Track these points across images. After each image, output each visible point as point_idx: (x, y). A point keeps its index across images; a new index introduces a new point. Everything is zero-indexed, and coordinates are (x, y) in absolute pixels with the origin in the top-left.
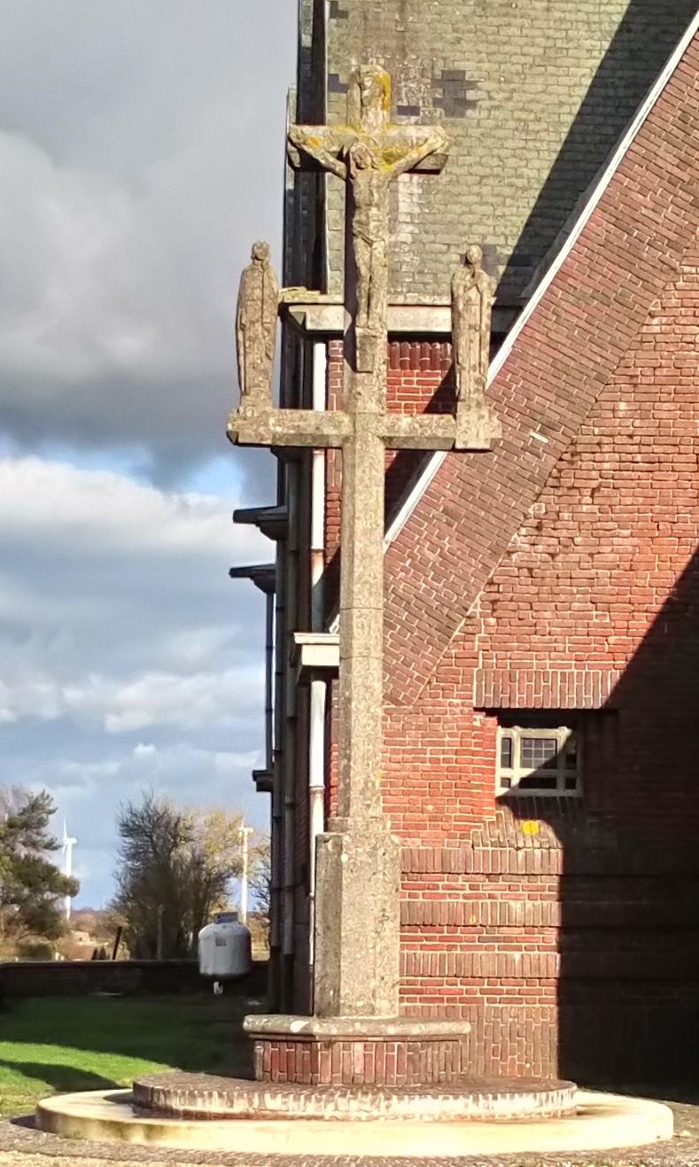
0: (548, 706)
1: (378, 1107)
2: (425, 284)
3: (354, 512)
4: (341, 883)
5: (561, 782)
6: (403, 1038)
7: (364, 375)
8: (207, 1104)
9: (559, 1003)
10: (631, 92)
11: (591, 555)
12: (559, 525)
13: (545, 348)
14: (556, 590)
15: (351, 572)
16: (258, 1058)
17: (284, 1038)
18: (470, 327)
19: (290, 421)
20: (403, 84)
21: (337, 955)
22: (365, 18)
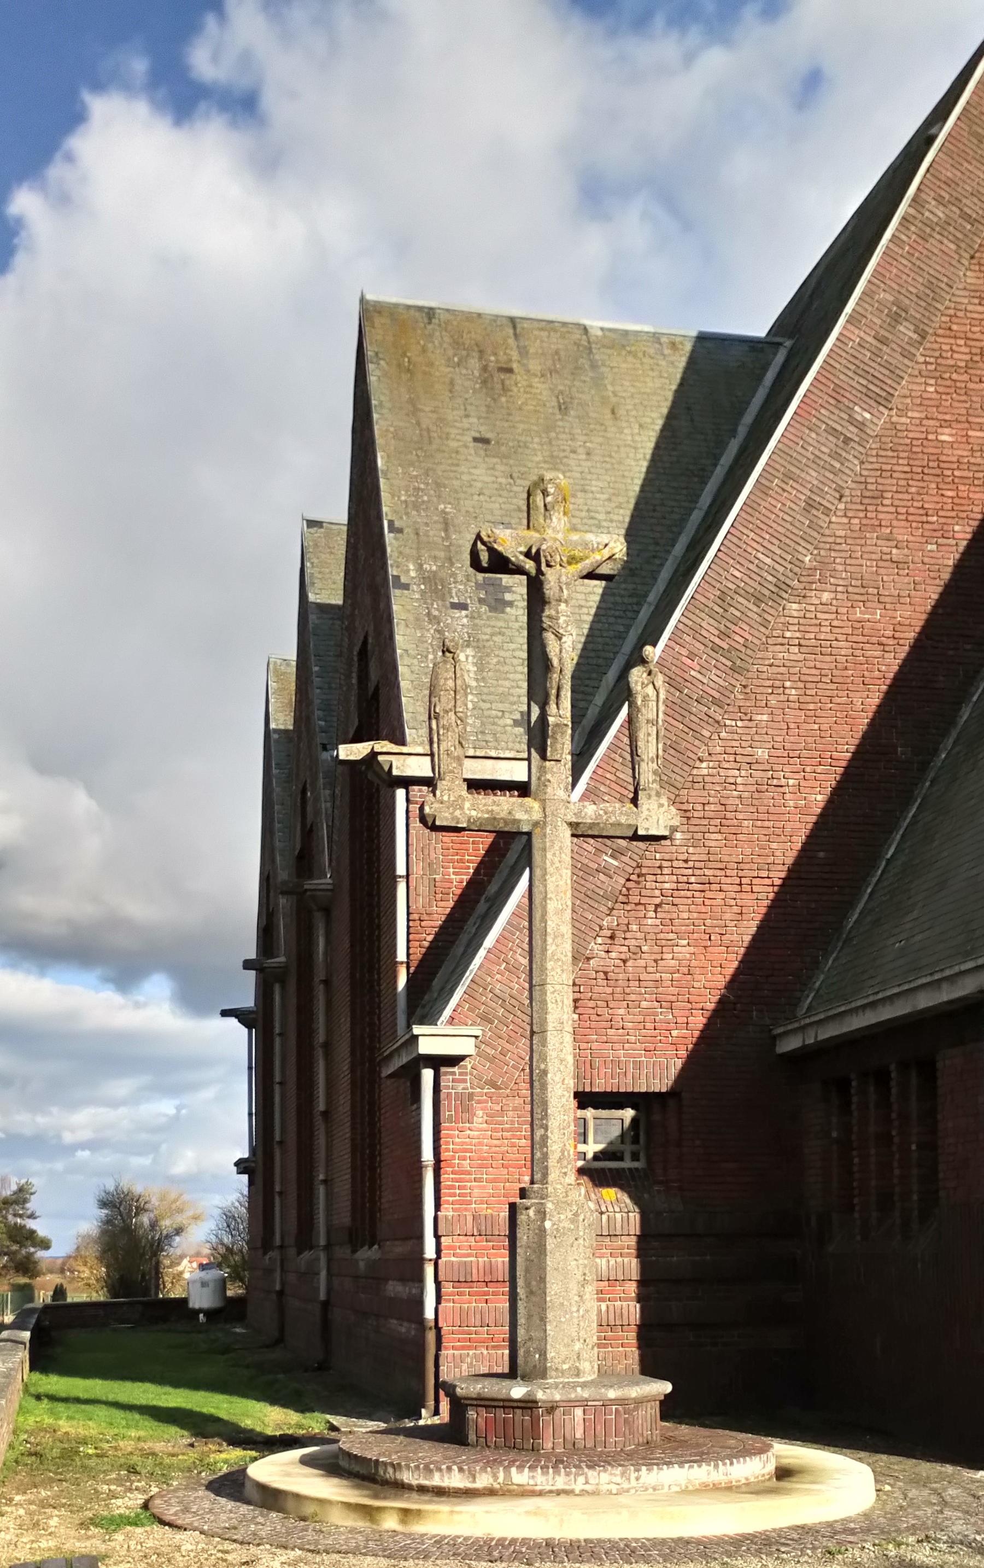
0: (622, 1090)
1: (629, 1479)
2: (487, 742)
3: (546, 892)
4: (545, 1249)
5: (627, 1156)
6: (621, 1401)
7: (553, 763)
8: (446, 1479)
9: (639, 1348)
10: (635, 600)
11: (656, 961)
12: (628, 935)
13: (614, 786)
14: (627, 990)
15: (544, 950)
16: (471, 1423)
17: (501, 1404)
18: (648, 721)
19: (485, 805)
20: (453, 585)
21: (543, 1320)
22: (417, 534)
